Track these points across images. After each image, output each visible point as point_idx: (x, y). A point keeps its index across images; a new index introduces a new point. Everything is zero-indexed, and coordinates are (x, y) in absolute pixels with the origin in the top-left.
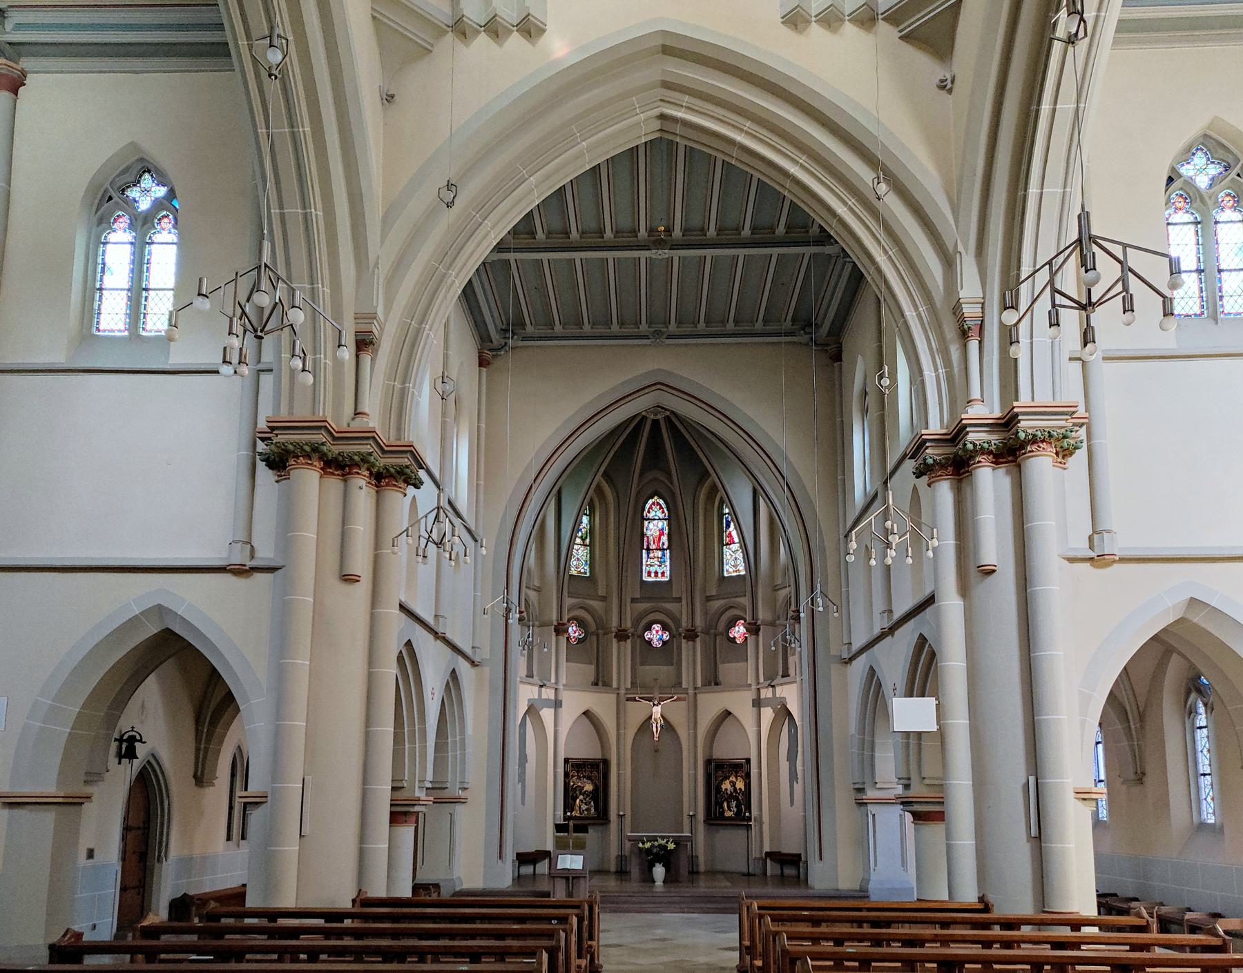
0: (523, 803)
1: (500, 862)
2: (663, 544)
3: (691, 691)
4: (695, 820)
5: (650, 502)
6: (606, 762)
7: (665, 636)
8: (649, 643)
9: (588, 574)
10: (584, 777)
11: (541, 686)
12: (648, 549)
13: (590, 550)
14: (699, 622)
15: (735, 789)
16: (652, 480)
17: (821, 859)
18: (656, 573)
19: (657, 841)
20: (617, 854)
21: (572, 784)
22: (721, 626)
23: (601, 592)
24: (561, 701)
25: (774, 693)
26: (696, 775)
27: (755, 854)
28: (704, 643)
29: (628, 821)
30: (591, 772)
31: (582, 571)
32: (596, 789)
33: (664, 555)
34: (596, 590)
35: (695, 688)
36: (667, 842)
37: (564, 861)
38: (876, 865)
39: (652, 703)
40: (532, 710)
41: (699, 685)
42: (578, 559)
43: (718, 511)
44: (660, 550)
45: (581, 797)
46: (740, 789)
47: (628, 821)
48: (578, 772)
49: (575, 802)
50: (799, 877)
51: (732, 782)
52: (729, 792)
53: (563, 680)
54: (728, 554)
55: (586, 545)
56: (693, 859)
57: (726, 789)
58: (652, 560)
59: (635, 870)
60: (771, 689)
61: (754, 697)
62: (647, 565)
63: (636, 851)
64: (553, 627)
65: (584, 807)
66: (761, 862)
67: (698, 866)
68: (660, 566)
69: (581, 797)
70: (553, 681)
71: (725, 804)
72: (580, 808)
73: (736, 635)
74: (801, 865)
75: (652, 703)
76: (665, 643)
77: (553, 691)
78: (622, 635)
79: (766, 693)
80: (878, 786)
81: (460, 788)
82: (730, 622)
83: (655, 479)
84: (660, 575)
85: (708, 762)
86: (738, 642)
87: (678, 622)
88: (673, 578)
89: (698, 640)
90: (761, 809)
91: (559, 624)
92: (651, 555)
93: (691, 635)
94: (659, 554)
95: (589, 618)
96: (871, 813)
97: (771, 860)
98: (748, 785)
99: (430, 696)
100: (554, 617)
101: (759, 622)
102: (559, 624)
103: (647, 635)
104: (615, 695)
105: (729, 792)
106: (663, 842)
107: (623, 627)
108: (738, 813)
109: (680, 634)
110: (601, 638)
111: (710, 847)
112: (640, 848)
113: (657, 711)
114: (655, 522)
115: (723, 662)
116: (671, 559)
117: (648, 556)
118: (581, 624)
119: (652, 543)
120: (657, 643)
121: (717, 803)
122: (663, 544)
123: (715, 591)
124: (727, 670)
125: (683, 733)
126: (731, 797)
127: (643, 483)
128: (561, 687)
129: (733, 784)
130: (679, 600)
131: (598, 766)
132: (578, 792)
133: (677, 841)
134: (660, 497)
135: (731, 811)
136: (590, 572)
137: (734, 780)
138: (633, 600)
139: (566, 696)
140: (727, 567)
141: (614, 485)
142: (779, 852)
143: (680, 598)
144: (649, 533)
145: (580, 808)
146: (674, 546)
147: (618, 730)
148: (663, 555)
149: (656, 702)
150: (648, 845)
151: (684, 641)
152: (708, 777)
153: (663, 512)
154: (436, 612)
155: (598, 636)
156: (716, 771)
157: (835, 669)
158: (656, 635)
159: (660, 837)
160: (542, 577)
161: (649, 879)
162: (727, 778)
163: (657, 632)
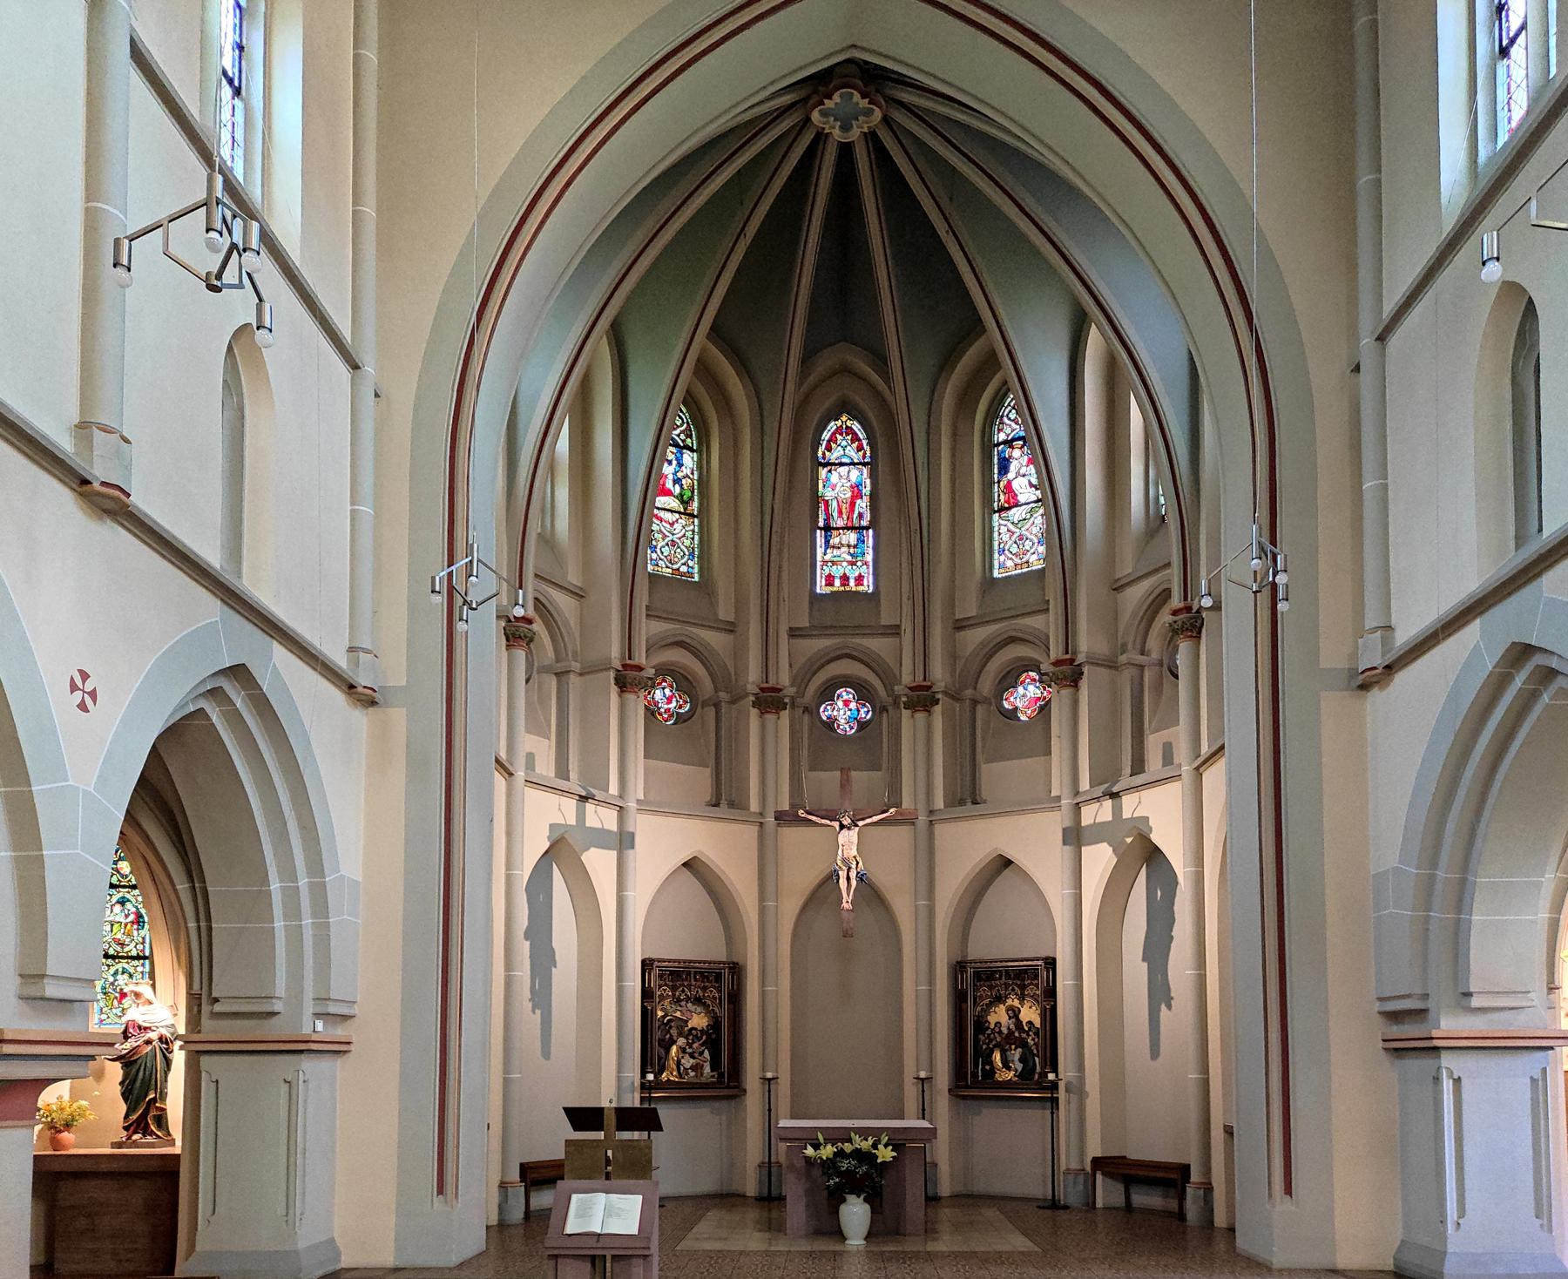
0: (546, 1054)
1: (438, 1201)
2: (861, 516)
3: (922, 819)
4: (931, 1087)
5: (832, 426)
6: (736, 970)
7: (863, 711)
8: (831, 724)
9: (696, 578)
10: (688, 999)
11: (584, 799)
12: (828, 528)
13: (700, 526)
14: (939, 673)
15: (1019, 1024)
16: (834, 373)
17: (1288, 1190)
18: (845, 579)
19: (850, 1140)
20: (758, 1161)
21: (660, 1014)
22: (986, 686)
23: (725, 612)
24: (633, 835)
25: (1117, 811)
26: (931, 993)
27: (1068, 1160)
28: (948, 717)
29: (784, 1089)
30: (704, 989)
31: (683, 569)
32: (715, 1025)
33: (861, 541)
34: (713, 605)
35: (931, 812)
36: (875, 1146)
37: (585, 1213)
38: (1462, 1212)
39: (836, 824)
40: (560, 850)
41: (939, 803)
42: (673, 543)
43: (983, 437)
44: (852, 528)
45: (681, 1041)
46: (1030, 1023)
47: (784, 1089)
48: (674, 989)
49: (668, 1050)
50: (1181, 1216)
51: (1011, 1009)
52: (1005, 1031)
53: (638, 790)
54: (1004, 530)
55: (692, 515)
56: (929, 1169)
57: (998, 1024)
58: (836, 552)
59: (796, 1211)
60: (1108, 803)
61: (1068, 823)
62: (825, 562)
63: (800, 1164)
64: (612, 674)
65: (688, 1062)
66: (1081, 1179)
67: (935, 1184)
68: (852, 564)
69: (681, 1041)
70: (614, 789)
71: (997, 1057)
72: (679, 1064)
73: (1019, 704)
74: (1190, 1191)
75: (836, 824)
76: (863, 725)
77: (614, 814)
78: (769, 700)
79: (1097, 813)
80: (1476, 1002)
81: (318, 1015)
82: (1004, 677)
83: (846, 370)
84: (852, 583)
85: (959, 967)
86: (1023, 718)
87: (888, 678)
88: (883, 591)
89: (938, 709)
90: (1081, 1067)
91: (625, 666)
92: (835, 541)
93: (922, 699)
94: (852, 537)
95: (699, 669)
96: (1450, 1073)
97: (1103, 1174)
98: (1050, 1016)
99: (62, 704)
100: (615, 653)
101: (1081, 658)
102: (625, 666)
103: (825, 712)
104: (754, 829)
105: (1005, 1031)
106: (866, 1145)
107: (772, 683)
108: (1026, 1075)
109: (896, 703)
110: (724, 708)
111: (962, 1143)
112: (808, 1159)
113: (849, 841)
114: (843, 470)
115: (990, 761)
116: (875, 548)
117: (827, 542)
118: (684, 683)
119: (835, 515)
120: (845, 726)
121: (978, 1053)
122: (861, 516)
123: (975, 610)
124: (996, 775)
125: (903, 907)
126: (1015, 1037)
127: (812, 379)
128: (632, 805)
129: (1014, 1013)
130: (894, 631)
131: (718, 977)
132: (674, 1032)
133: (899, 1141)
134: (854, 418)
135: (1009, 1069)
136: (701, 576)
137: (1016, 1003)
138: (794, 633)
139: (644, 826)
140: (1002, 558)
141: (745, 366)
142: (1125, 1157)
143: (898, 627)
144: (829, 494)
145: (679, 1064)
146: (883, 520)
147: (762, 897)
148: (861, 541)
149: (846, 821)
150: (828, 1151)
151: (906, 713)
152: (959, 998)
153: (860, 448)
154: (82, 412)
155: (717, 705)
156: (976, 988)
157: (1333, 704)
158: (844, 711)
159: (859, 1131)
160: (588, 565)
161: (839, 1234)
162: (1000, 999)
163: (846, 703)
